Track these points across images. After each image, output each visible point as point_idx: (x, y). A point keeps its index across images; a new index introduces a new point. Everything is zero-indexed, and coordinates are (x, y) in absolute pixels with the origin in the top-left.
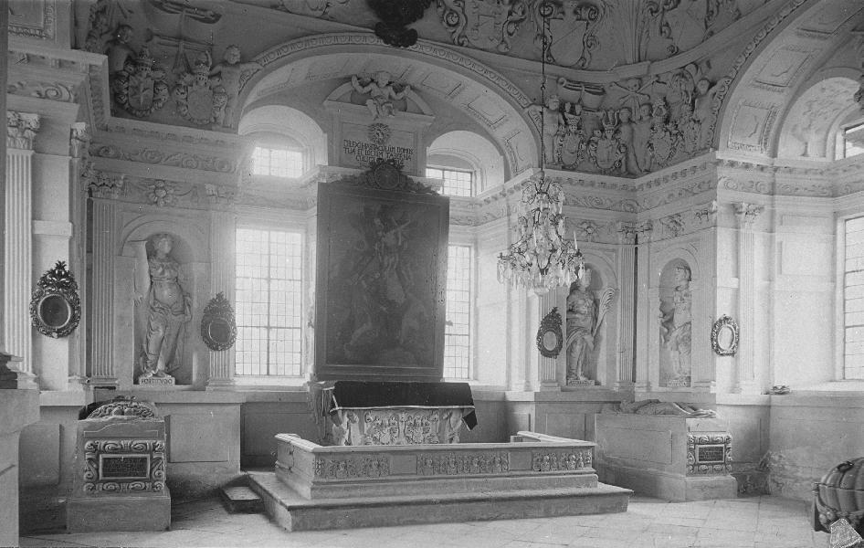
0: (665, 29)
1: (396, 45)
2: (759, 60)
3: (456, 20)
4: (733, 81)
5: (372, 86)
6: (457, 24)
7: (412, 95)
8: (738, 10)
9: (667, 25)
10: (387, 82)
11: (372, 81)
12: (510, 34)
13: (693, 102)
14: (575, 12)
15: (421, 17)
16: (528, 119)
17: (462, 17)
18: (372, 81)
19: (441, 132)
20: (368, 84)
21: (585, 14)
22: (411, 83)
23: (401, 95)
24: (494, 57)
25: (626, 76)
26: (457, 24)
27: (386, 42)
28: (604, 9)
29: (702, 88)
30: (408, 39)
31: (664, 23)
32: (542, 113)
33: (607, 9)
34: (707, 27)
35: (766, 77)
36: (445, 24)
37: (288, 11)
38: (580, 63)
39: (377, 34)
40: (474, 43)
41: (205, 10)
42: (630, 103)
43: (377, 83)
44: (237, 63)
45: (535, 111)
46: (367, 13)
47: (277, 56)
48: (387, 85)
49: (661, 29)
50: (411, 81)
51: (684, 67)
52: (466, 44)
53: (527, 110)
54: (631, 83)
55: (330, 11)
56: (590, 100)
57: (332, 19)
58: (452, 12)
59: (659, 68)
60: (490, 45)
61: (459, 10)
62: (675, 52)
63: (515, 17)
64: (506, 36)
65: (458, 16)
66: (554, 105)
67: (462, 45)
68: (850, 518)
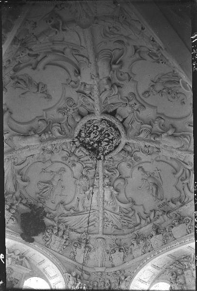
0: (111, 259)
2: (139, 273)
3: (48, 239)
4: (131, 279)
5: (12, 254)
7: (26, 261)
10: (18, 254)
13: (119, 283)
15: (37, 235)
16: (64, 276)
18: (13, 252)
19: (32, 276)
20: (10, 253)
21: (87, 249)
23: (22, 260)
24: (56, 253)
25: (98, 271)
29: (123, 278)
30: (32, 241)
32: (105, 90)
35: (142, 278)
39: (23, 222)
40: (52, 248)
42: (98, 280)
50: (27, 256)
54: (99, 273)
56: (86, 276)
58: (47, 237)
59: (108, 271)
60: (56, 250)
62: (113, 266)
63: (67, 244)
66: (74, 274)
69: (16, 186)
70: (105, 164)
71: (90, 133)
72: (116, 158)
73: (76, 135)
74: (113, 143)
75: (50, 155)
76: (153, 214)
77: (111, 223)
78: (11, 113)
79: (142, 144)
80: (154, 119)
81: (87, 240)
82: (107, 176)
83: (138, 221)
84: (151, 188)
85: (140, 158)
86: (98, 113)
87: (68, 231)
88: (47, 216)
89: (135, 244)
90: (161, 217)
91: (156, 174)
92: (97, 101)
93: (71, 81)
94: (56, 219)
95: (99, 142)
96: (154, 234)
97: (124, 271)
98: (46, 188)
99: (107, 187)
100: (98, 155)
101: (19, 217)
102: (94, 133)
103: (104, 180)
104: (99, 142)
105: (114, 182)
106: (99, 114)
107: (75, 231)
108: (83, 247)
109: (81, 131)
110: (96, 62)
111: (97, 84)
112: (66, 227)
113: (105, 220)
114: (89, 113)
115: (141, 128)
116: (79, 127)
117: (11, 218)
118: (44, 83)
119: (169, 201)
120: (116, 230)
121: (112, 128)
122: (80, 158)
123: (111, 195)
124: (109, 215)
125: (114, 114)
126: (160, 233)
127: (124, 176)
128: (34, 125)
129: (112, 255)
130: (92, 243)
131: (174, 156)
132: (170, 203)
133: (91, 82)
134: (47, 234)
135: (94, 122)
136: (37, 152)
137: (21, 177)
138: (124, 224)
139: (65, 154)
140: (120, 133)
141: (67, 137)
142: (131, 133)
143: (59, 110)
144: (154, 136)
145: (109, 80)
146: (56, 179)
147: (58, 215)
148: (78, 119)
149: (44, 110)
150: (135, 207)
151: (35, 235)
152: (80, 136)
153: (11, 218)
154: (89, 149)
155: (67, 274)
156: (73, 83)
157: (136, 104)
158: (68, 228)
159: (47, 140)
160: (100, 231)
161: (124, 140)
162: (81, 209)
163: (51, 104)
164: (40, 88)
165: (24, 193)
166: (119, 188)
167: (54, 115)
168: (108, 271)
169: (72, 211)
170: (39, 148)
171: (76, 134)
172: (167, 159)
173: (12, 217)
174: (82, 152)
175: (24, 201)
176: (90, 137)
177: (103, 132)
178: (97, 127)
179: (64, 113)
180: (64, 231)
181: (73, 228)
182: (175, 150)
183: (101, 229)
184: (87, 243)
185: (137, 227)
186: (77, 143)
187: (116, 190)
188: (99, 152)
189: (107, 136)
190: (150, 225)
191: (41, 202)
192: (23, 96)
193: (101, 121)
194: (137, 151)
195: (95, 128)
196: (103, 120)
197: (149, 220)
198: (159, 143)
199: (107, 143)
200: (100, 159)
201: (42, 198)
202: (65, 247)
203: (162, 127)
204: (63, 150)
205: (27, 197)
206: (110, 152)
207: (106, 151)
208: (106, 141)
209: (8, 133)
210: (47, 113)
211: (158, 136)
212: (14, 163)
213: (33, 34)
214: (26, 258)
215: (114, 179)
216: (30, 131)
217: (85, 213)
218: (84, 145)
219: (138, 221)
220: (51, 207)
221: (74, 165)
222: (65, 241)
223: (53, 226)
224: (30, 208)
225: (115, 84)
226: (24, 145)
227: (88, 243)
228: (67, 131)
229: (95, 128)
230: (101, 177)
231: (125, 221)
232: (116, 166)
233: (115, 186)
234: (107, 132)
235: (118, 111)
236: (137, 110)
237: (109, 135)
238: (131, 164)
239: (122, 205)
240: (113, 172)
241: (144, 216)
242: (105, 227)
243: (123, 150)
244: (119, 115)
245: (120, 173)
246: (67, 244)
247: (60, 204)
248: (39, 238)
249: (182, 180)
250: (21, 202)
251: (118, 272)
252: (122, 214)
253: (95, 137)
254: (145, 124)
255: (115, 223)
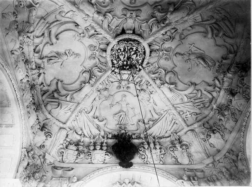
1: (126, 167)
3: (144, 157)
6: (145, 158)
8: (229, 131)
9: (211, 144)
10: (128, 182)
11: (124, 183)
12: (163, 158)
14: (181, 148)
17: (145, 155)
18: (124, 183)
20: (122, 184)
21: (184, 147)
22: (137, 181)
26: (145, 158)
27: (123, 167)
28: (189, 144)
31: (210, 143)
32: (183, 182)
33: (190, 144)
34: (224, 140)
36: (141, 159)
37: (93, 164)
38: (190, 163)
41: (69, 168)
43: (125, 183)
44: (76, 182)
45: (180, 182)
46: (116, 160)
47: (89, 178)
48: (129, 183)
49: (210, 146)
51: (225, 155)
52: (149, 163)
53: (177, 182)
55: (106, 161)
57: (106, 163)
58: (142, 155)
61: (144, 154)
63: (163, 152)
64: (161, 159)
65: (144, 155)
67: (148, 164)
68: (221, 162)
69: (98, 128)
70: (147, 71)
71: (119, 57)
72: (152, 61)
73: (111, 65)
74: (139, 52)
75: (106, 92)
76: (217, 82)
77: (188, 113)
78: (62, 81)
79: (159, 35)
80: (153, 11)
81: (179, 139)
82: (156, 79)
83: (210, 97)
84: (198, 63)
85: (171, 48)
86: (111, 40)
87: (157, 140)
88: (133, 136)
89: (222, 118)
90: (225, 79)
91: (193, 49)
92: (102, 32)
93: (80, 34)
94: (142, 136)
95: (129, 58)
96: (231, 98)
97: (232, 150)
98: (120, 117)
99: (162, 86)
100: (137, 68)
101: (110, 150)
102: (121, 55)
103: (156, 83)
104: (129, 58)
105: (165, 79)
106: (112, 40)
107: (163, 138)
108: (179, 148)
109: (112, 60)
110: (78, 8)
111: (92, 22)
112: (154, 138)
113: (181, 113)
114: (108, 45)
115: (149, 26)
116: (109, 59)
117: (106, 154)
118: (68, 49)
119: (222, 61)
120: (197, 116)
121: (130, 42)
122: (129, 80)
123: (171, 90)
124: (181, 108)
125: (123, 32)
126: (237, 93)
127: (169, 70)
128: (82, 79)
129: (210, 140)
130: (185, 139)
131: (191, 23)
132: (224, 61)
133: (88, 24)
134: (141, 152)
135: (115, 47)
136: (96, 94)
137: (98, 119)
138: (199, 107)
139: (116, 84)
140: (139, 41)
141: (106, 71)
142: (145, 35)
143: (89, 58)
144: (162, 22)
145: (99, 13)
146: (124, 105)
147: (142, 132)
148: (104, 55)
149: (81, 65)
150: (197, 87)
151: (130, 160)
152: (114, 64)
153: (106, 154)
154: (128, 69)
155: (179, 181)
156: (82, 35)
157: (132, 14)
158: (156, 138)
159: (95, 83)
160: (184, 126)
161: (145, 44)
162: (156, 117)
163: (82, 58)
164: (68, 54)
165: (107, 130)
166: (172, 81)
167: (89, 64)
168: (217, 158)
169: (151, 123)
170: (95, 91)
171: (110, 64)
172: (189, 30)
173: (106, 153)
174: (126, 74)
175: (110, 136)
176: (120, 60)
177: (126, 50)
178: (119, 49)
179: (94, 58)
180: (155, 142)
181: (161, 135)
182: (187, 18)
183: (184, 124)
184: (180, 142)
185: (214, 102)
186: (117, 70)
187: (172, 84)
188: (135, 65)
189: (131, 50)
190: (222, 92)
191: (122, 130)
192: (62, 66)
193: (118, 43)
194: (163, 44)
195: (119, 51)
196: (119, 42)
197: (218, 89)
198: (170, 23)
199: (135, 55)
200: (140, 70)
201: (122, 125)
202: (162, 156)
203: (162, 11)
204: (112, 82)
205: (110, 131)
206: (143, 59)
207: (140, 61)
208: (134, 54)
209: (68, 95)
210: (84, 65)
211: (165, 19)
212: (86, 112)
213: (23, 22)
214: (137, 183)
215: (163, 77)
216: (81, 85)
217: (161, 118)
218: (122, 68)
219: (210, 97)
220: (132, 129)
221: (128, 87)
222: (159, 150)
223: (143, 143)
224: (116, 139)
225: (106, 12)
226: (83, 96)
227: (182, 142)
228: (104, 67)
229: (119, 51)
230: (152, 82)
231: (199, 104)
232: (157, 66)
233: (168, 81)
234: (129, 48)
235: (125, 29)
236: (137, 16)
237: (132, 49)
238: (168, 57)
239: (187, 92)
240: (158, 72)
241: (210, 88)
242: (185, 119)
243: (151, 52)
244: (128, 30)
245: (164, 70)
246: (163, 152)
247: (139, 122)
248: (136, 160)
249: (216, 36)
250: (107, 138)
251: (227, 154)
252: (192, 100)
253: (124, 57)
254: (149, 20)
255: (192, 111)
